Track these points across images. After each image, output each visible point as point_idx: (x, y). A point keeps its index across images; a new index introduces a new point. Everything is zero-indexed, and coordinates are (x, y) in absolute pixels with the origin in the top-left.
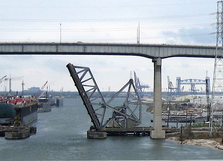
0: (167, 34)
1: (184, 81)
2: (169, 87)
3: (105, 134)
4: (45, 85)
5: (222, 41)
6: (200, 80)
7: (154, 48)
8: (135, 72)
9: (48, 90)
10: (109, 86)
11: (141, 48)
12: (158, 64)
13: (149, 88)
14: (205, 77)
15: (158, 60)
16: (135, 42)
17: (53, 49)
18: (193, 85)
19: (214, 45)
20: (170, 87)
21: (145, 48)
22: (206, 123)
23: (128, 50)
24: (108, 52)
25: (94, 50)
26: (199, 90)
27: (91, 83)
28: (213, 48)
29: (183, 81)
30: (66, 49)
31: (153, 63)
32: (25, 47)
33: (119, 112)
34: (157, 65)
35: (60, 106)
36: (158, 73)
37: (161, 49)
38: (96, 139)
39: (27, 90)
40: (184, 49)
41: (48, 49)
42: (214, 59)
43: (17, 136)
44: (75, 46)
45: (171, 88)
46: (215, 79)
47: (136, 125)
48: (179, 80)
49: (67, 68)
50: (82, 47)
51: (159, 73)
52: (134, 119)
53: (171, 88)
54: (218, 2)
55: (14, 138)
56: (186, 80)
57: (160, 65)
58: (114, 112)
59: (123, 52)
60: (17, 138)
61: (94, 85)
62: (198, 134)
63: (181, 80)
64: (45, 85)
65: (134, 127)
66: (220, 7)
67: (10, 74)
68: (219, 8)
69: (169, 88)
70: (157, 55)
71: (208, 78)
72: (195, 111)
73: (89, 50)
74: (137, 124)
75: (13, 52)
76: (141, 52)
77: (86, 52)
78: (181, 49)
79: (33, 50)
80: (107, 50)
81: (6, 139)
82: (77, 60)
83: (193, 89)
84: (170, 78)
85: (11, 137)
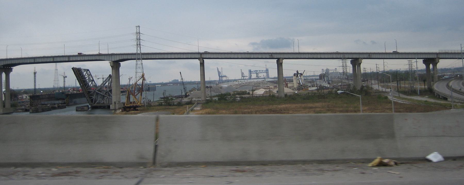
0: (253, 44)
2: (242, 75)
3: (20, 106)
6: (262, 71)
8: (218, 68)
9: (184, 81)
12: (281, 62)
15: (281, 60)
16: (97, 53)
18: (257, 74)
19: (135, 51)
24: (82, 60)
26: (261, 77)
28: (135, 54)
31: (110, 64)
33: (103, 94)
35: (150, 91)
37: (113, 56)
39: (171, 81)
40: (126, 56)
45: (243, 76)
49: (72, 69)
50: (67, 57)
53: (243, 76)
57: (282, 62)
58: (87, 92)
67: (103, 75)
69: (242, 76)
73: (71, 59)
77: (70, 60)
79: (40, 61)
80: (160, 56)
84: (242, 71)
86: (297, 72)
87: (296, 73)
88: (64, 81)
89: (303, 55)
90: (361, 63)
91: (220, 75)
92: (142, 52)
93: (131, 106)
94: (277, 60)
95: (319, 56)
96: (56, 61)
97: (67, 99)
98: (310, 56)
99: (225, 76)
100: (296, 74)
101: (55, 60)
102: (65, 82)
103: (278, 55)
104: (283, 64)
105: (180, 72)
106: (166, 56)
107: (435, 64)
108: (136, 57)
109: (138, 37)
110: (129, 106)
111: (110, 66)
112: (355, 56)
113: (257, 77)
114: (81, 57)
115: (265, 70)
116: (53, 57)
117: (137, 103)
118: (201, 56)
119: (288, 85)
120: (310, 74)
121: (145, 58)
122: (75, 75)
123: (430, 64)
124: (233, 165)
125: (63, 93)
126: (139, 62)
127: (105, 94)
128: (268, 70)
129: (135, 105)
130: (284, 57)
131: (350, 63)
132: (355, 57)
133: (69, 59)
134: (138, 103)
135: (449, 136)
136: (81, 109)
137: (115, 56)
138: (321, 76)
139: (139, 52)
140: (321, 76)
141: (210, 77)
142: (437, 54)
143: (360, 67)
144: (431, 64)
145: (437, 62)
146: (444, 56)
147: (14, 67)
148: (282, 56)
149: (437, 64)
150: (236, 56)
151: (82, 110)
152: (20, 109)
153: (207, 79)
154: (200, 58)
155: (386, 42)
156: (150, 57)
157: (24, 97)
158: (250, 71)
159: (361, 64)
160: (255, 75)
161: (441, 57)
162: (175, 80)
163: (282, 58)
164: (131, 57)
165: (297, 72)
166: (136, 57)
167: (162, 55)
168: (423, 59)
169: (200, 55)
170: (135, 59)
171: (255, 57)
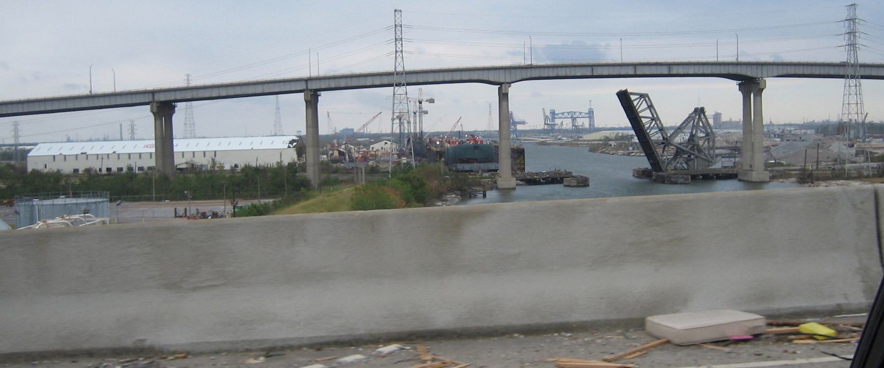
1: (566, 114)
4: (458, 122)
5: (397, 66)
6: (580, 113)
7: (755, 66)
10: (335, 127)
11: (739, 68)
13: (526, 124)
14: (588, 108)
16: (733, 59)
17: (631, 71)
18: (574, 119)
20: (546, 123)
21: (744, 68)
22: (771, 163)
23: (708, 70)
25: (681, 70)
27: (647, 113)
29: (558, 114)
30: (647, 70)
32: (595, 68)
33: (687, 150)
34: (503, 92)
36: (758, 98)
37: (765, 68)
38: (681, 183)
41: (623, 71)
42: (393, 87)
43: (582, 183)
44: (658, 66)
46: (849, 104)
47: (709, 166)
48: (553, 113)
51: (506, 103)
52: (706, 158)
54: (395, 11)
55: (579, 185)
56: (563, 113)
59: (701, 72)
60: (582, 185)
61: (651, 116)
62: (251, 196)
63: (556, 113)
64: (458, 122)
65: (706, 168)
66: (398, 18)
68: (396, 18)
69: (545, 124)
70: (502, 81)
71: (592, 110)
72: (672, 150)
73: (675, 71)
74: (710, 164)
75: (580, 75)
76: (481, 78)
78: (697, 67)
81: (565, 186)
82: (633, 86)
83: (546, 123)
85: (575, 184)
90: (762, 90)
94: (499, 88)
95: (223, 92)
98: (448, 77)
99: (523, 123)
101: (638, 73)
106: (362, 82)
109: (399, 46)
111: (305, 100)
112: (162, 98)
114: (637, 70)
115: (588, 112)
116: (670, 65)
120: (129, 130)
126: (400, 90)
127: (691, 149)
128: (593, 112)
133: (670, 71)
136: (685, 180)
141: (335, 127)
148: (171, 97)
150: (377, 81)
151: (685, 182)
152: (667, 167)
153: (324, 129)
155: (92, 65)
156: (343, 85)
159: (764, 90)
162: (347, 129)
164: (329, 85)
167: (19, 105)
171: (534, 76)
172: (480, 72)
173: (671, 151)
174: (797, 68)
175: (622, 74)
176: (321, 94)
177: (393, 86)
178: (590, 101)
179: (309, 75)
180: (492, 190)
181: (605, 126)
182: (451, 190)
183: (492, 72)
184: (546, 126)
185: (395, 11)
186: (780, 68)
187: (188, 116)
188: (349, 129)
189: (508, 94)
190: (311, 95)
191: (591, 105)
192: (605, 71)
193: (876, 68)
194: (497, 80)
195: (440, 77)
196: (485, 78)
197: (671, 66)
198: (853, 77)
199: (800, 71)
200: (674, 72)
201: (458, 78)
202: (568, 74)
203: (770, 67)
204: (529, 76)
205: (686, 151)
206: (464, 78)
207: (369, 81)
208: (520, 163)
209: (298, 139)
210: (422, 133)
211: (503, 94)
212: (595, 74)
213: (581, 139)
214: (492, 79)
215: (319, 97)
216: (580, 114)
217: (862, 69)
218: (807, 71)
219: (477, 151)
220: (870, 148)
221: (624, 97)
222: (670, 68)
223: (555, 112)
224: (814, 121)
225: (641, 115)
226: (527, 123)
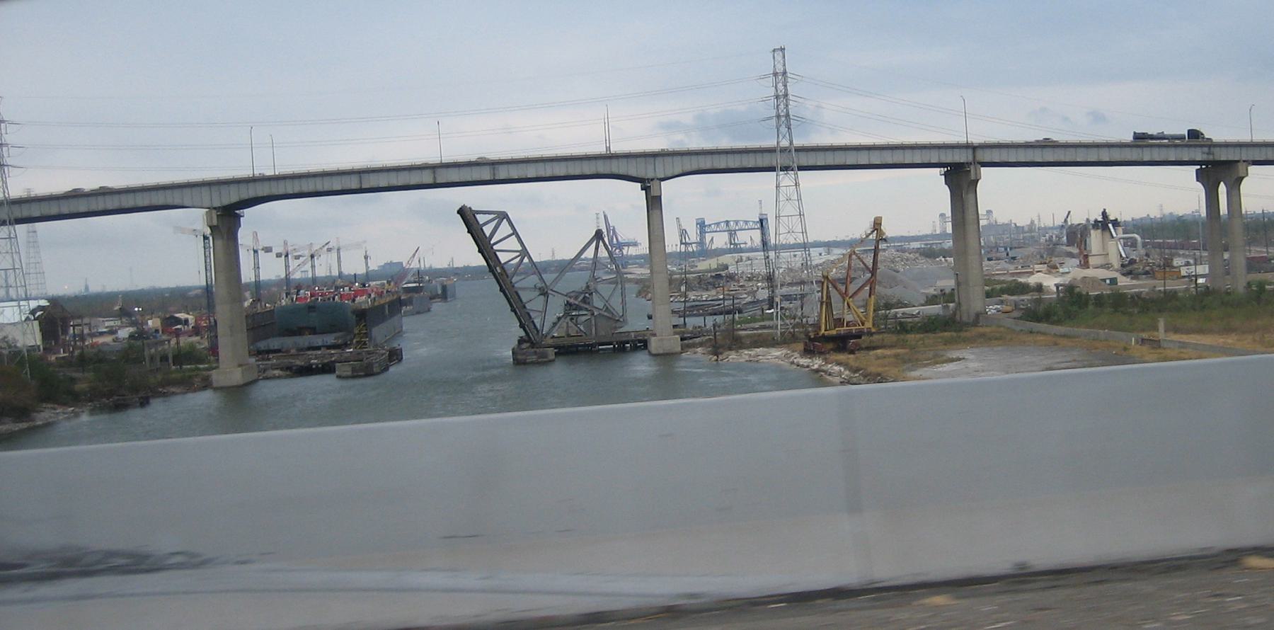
1: (722, 224)
2: (681, 241)
4: (414, 255)
6: (746, 222)
16: (600, 149)
17: (427, 178)
18: (732, 233)
21: (623, 162)
25: (515, 172)
29: (710, 225)
30: (454, 176)
32: (365, 176)
33: (577, 303)
35: (449, 300)
39: (377, 269)
42: (775, 173)
47: (616, 328)
49: (459, 215)
54: (774, 51)
55: (355, 374)
56: (718, 224)
59: (549, 174)
60: (362, 374)
64: (414, 255)
69: (682, 243)
70: (650, 175)
71: (765, 217)
73: (502, 173)
74: (618, 324)
76: (615, 171)
78: (701, 158)
82: (480, 198)
85: (349, 373)
86: (1104, 214)
87: (1100, 219)
88: (367, 264)
89: (910, 151)
91: (615, 240)
92: (798, 142)
93: (842, 332)
94: (1197, 170)
96: (368, 187)
97: (362, 330)
100: (1100, 222)
102: (258, 268)
103: (1231, 150)
104: (1243, 183)
105: (1069, 212)
106: (851, 159)
107: (1235, 186)
108: (778, 160)
110: (834, 332)
113: (731, 244)
116: (360, 173)
117: (863, 324)
118: (974, 157)
119: (1088, 262)
120: (909, 232)
121: (1108, 160)
122: (469, 235)
123: (1219, 183)
124: (1191, 558)
125: (311, 308)
126: (787, 179)
127: (581, 301)
129: (854, 332)
130: (1251, 158)
131: (1195, 180)
132: (948, 161)
133: (494, 174)
134: (866, 323)
135: (525, 592)
136: (539, 358)
137: (665, 158)
138: (1075, 233)
139: (785, 143)
140: (1075, 233)
142: (973, 148)
143: (658, 212)
144: (1222, 183)
145: (1241, 175)
146: (996, 156)
147: (245, 210)
149: (1241, 181)
150: (1093, 157)
151: (540, 360)
154: (971, 164)
157: (1182, 272)
158: (702, 225)
159: (980, 181)
160: (725, 236)
161: (987, 159)
162: (391, 264)
163: (1244, 161)
165: (1104, 214)
166: (778, 160)
168: (1199, 167)
169: (970, 151)
170: (772, 169)
172: (169, 192)
173: (556, 308)
174: (745, 157)
175: (412, 183)
176: (243, 212)
177: (775, 171)
178: (760, 201)
179: (546, 166)
180: (206, 389)
181: (835, 239)
182: (743, 337)
183: (187, 191)
184: (682, 246)
185: (782, 49)
186: (686, 159)
187: (32, 260)
188: (394, 263)
189: (660, 196)
190: (218, 215)
191: (761, 208)
192: (383, 181)
193: (855, 152)
194: (641, 174)
195: (548, 170)
196: (622, 171)
197: (496, 166)
198: (786, 169)
199: (749, 161)
200: (502, 175)
201: (101, 207)
202: (320, 188)
203: (668, 159)
204: (695, 167)
205: (575, 304)
206: (732, 165)
207: (863, 158)
208: (359, 334)
209: (48, 304)
210: (1164, 215)
211: (654, 197)
212: (365, 186)
213: (600, 280)
214: (633, 173)
215: (242, 218)
216: (737, 224)
217: (802, 155)
218: (733, 162)
219: (314, 314)
220: (1005, 274)
221: (467, 215)
222: (494, 169)
223: (704, 223)
224: (1148, 215)
225: (495, 247)
226: (640, 244)
